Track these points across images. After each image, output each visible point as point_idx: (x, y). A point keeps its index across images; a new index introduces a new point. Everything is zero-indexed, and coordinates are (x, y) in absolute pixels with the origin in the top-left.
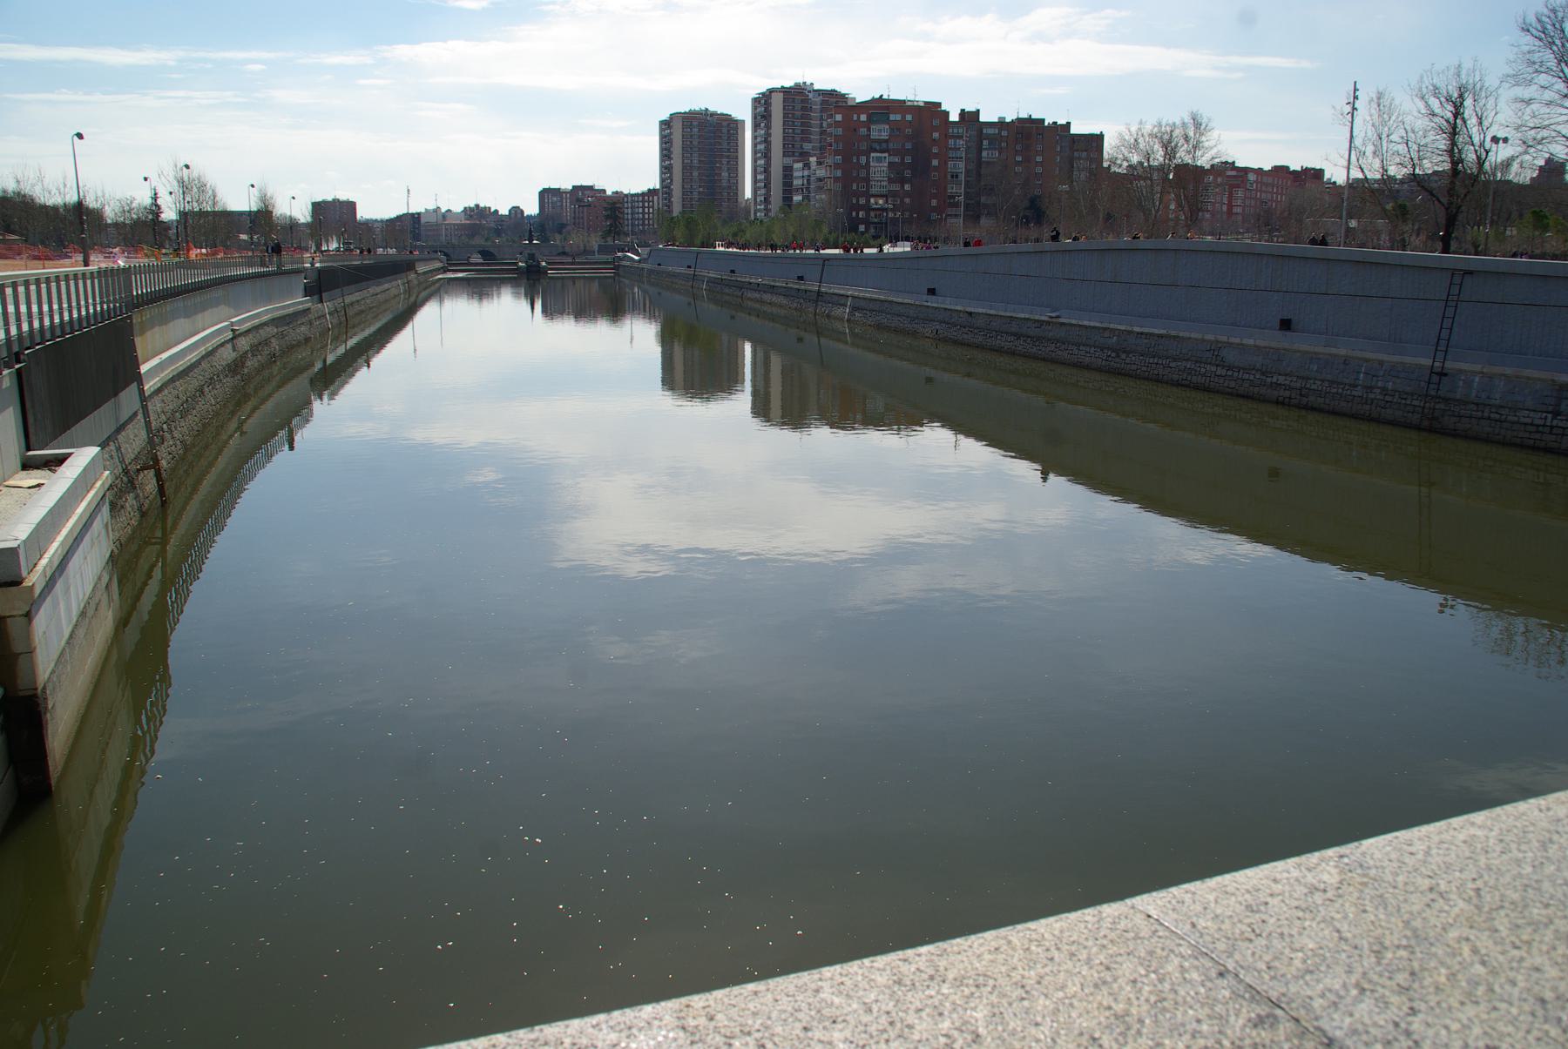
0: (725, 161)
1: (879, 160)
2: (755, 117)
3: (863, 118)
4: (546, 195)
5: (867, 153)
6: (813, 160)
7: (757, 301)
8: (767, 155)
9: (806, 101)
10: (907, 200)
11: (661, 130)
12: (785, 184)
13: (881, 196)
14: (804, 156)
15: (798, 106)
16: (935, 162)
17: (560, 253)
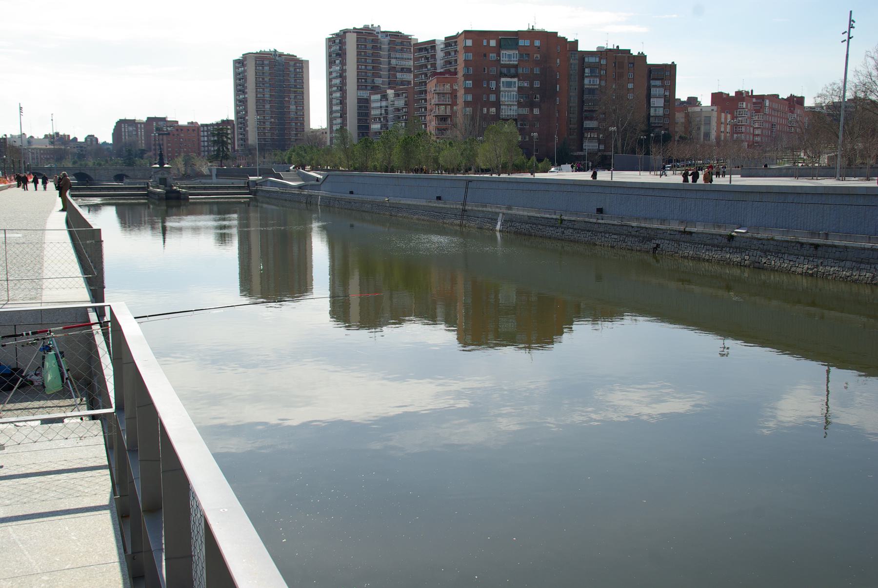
0: (292, 96)
1: (509, 85)
3: (493, 43)
5: (497, 78)
8: (342, 88)
9: (376, 41)
11: (235, 68)
14: (375, 89)
15: (369, 46)
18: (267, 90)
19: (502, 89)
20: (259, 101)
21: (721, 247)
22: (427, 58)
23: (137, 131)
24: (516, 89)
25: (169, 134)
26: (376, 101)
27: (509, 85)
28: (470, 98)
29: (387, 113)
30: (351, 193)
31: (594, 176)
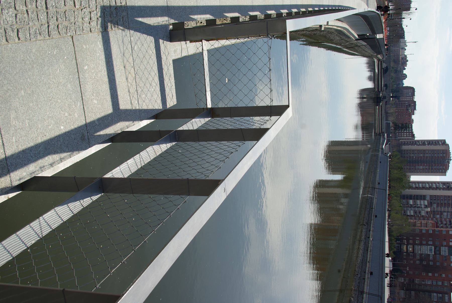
1: (431, 250)
2: (448, 183)
4: (412, 90)
6: (429, 209)
7: (361, 237)
8: (430, 188)
10: (412, 262)
11: (441, 141)
12: (417, 196)
13: (413, 250)
14: (430, 204)
16: (430, 274)
17: (388, 101)
18: (430, 155)
19: (429, 247)
20: (424, 151)
21: (366, 235)
22: (446, 224)
23: (409, 97)
24: (429, 253)
25: (407, 110)
26: (424, 203)
27: (431, 250)
28: (424, 232)
29: (418, 207)
30: (380, 162)
31: (388, 255)
